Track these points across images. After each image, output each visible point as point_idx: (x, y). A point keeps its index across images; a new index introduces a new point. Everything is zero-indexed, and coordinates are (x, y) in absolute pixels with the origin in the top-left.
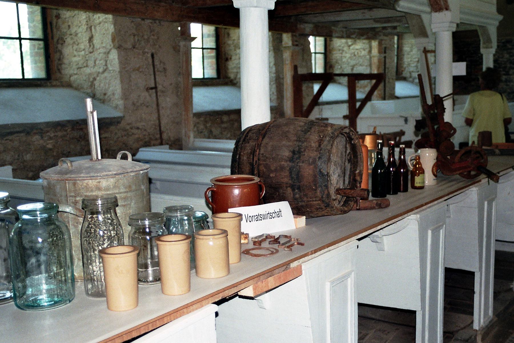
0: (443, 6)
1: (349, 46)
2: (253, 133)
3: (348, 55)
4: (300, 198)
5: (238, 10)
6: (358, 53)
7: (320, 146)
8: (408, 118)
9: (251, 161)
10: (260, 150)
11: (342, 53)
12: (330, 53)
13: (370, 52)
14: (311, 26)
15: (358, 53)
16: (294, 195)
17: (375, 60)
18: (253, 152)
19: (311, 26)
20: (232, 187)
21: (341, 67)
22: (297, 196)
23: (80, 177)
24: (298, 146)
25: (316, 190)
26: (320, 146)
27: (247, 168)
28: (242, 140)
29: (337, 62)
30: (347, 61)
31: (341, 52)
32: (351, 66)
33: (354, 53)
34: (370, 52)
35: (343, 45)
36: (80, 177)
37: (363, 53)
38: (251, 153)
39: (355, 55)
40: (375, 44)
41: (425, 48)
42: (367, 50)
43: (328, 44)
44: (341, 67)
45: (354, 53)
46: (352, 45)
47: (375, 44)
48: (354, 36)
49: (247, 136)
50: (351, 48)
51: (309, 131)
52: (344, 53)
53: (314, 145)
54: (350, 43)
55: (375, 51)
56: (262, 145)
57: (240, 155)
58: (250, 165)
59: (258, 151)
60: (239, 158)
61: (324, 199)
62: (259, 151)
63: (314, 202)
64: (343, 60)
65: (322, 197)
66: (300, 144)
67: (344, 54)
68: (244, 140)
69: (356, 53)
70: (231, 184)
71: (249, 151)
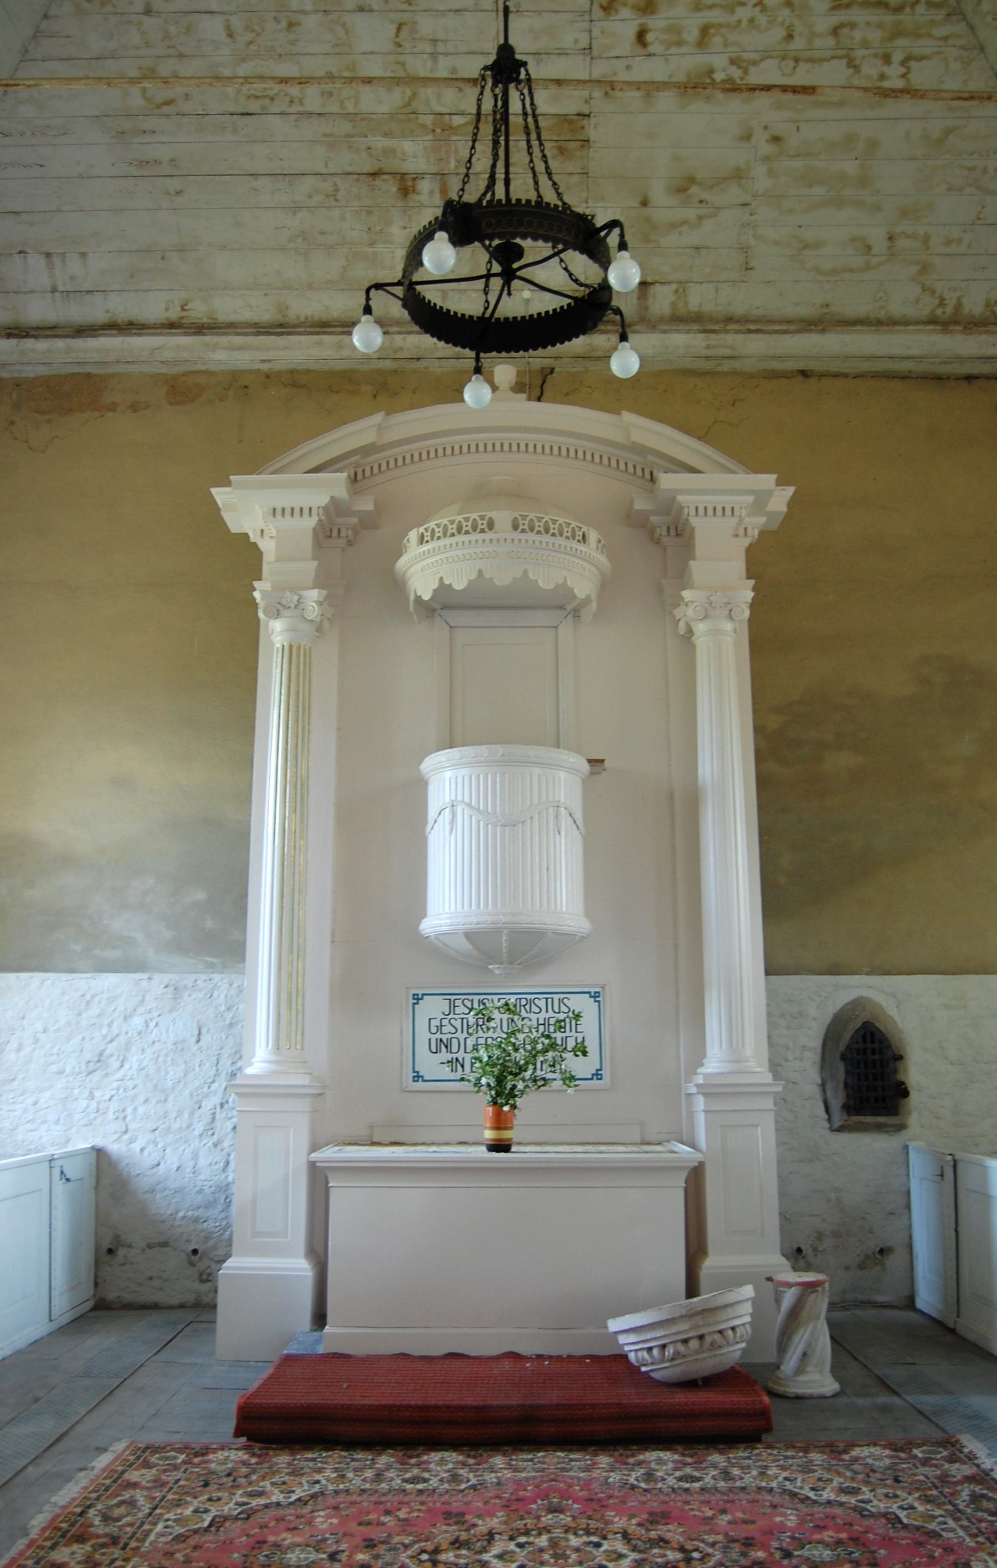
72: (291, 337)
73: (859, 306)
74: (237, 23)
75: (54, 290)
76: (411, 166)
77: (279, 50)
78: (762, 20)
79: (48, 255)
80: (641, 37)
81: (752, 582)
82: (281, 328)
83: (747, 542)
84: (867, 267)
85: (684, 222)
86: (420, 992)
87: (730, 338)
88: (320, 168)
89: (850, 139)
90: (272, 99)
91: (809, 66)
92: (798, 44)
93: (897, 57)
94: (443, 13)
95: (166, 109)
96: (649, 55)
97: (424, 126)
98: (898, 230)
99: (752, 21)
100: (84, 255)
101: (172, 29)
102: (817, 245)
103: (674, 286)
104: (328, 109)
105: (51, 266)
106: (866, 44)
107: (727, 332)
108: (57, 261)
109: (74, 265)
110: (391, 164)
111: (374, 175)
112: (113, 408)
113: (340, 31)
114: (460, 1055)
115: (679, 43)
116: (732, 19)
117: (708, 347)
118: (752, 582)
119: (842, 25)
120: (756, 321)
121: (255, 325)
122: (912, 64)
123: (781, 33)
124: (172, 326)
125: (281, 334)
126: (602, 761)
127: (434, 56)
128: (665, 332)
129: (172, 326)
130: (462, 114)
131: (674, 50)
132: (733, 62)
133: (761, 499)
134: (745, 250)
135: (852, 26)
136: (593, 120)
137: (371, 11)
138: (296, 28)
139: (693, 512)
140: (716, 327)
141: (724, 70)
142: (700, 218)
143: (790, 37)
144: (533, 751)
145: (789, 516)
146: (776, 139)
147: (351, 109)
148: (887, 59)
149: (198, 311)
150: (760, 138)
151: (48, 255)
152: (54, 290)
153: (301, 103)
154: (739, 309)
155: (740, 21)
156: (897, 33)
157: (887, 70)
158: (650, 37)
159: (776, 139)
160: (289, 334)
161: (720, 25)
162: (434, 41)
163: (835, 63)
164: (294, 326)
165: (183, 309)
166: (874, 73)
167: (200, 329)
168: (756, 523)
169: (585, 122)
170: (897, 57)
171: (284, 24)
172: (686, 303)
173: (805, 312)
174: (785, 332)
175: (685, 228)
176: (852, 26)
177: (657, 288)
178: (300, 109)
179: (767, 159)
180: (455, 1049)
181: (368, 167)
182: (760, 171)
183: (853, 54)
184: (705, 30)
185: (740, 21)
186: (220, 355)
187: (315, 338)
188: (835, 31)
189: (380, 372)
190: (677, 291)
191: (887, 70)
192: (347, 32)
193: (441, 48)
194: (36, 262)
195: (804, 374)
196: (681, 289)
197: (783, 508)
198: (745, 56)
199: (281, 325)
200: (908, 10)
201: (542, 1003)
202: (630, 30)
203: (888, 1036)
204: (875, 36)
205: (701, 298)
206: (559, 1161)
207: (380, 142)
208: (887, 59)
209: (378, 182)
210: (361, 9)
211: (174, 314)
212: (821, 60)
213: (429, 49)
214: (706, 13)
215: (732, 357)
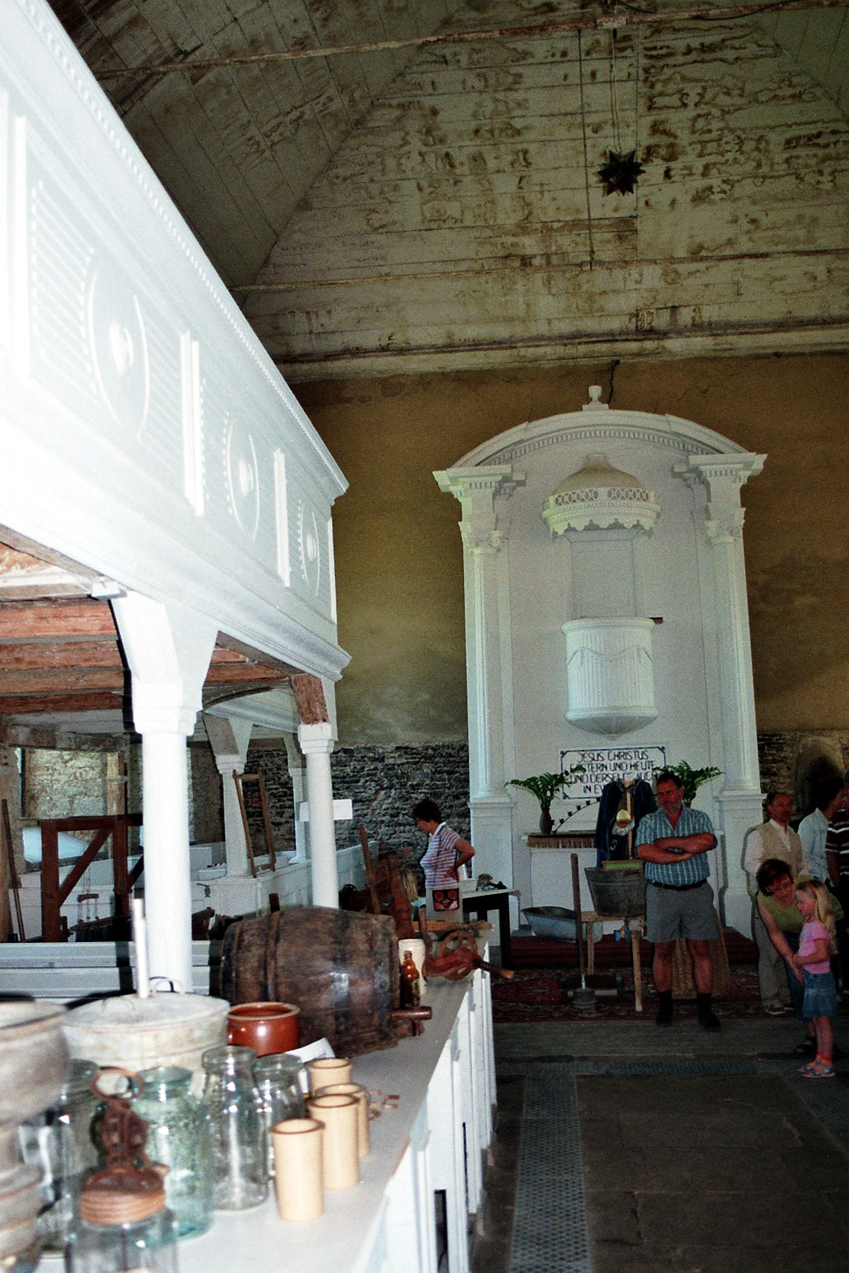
0: (320, 717)
1: (67, 762)
2: (252, 935)
3: (64, 778)
4: (346, 1029)
5: (140, 736)
6: (81, 773)
7: (371, 947)
8: (211, 888)
9: (262, 979)
10: (276, 960)
11: (52, 775)
12: (31, 773)
13: (103, 772)
14: (27, 730)
15: (81, 773)
16: (338, 1026)
17: (114, 787)
18: (264, 965)
19: (27, 730)
20: (256, 1023)
21: (51, 798)
22: (342, 1027)
23: (164, 1024)
24: (340, 951)
25: (372, 1015)
26: (371, 947)
27: (255, 992)
28: (235, 946)
29: (43, 790)
30: (62, 787)
31: (50, 771)
32: (69, 797)
33: (75, 773)
34: (103, 772)
35: (54, 761)
36: (164, 1024)
37: (91, 774)
38: (259, 967)
39: (76, 778)
40: (112, 759)
41: (234, 771)
42: (98, 770)
43: (27, 759)
44: (51, 798)
45: (75, 773)
46: (71, 759)
47: (112, 759)
48: (85, 747)
49: (243, 941)
50: (69, 764)
51: (347, 927)
52: (56, 773)
53: (363, 947)
54: (67, 758)
55: (113, 771)
56: (279, 952)
57: (237, 972)
58: (261, 986)
59: (272, 963)
60: (237, 976)
61: (383, 1028)
62: (276, 963)
63: (367, 1034)
64: (55, 787)
65: (381, 1025)
66: (342, 947)
67: (56, 776)
68: (239, 947)
69: (78, 774)
70: (253, 1019)
71: (256, 964)
72: (457, 354)
73: (812, 312)
74: (424, 183)
75: (311, 332)
76: (528, 252)
77: (449, 195)
78: (742, 159)
79: (308, 313)
80: (667, 174)
81: (744, 509)
82: (450, 347)
83: (741, 485)
84: (815, 288)
85: (698, 271)
86: (565, 750)
87: (730, 339)
88: (474, 256)
89: (800, 218)
90: (444, 221)
91: (772, 180)
92: (764, 170)
93: (827, 170)
94: (545, 170)
95: (380, 231)
96: (673, 182)
97: (537, 229)
98: (833, 266)
99: (735, 159)
100: (329, 312)
101: (386, 189)
102: (781, 279)
103: (693, 307)
104: (478, 224)
105: (309, 320)
106: (807, 166)
107: (727, 335)
108: (313, 316)
109: (324, 319)
110: (514, 251)
111: (506, 257)
112: (349, 401)
113: (486, 184)
114: (588, 784)
115: (691, 175)
116: (723, 160)
117: (715, 345)
118: (744, 509)
119: (791, 157)
120: (744, 325)
121: (433, 347)
122: (836, 174)
123: (754, 164)
124: (383, 350)
125: (451, 352)
126: (661, 619)
127: (542, 193)
128: (689, 337)
129: (383, 350)
130: (559, 221)
131: (687, 178)
132: (724, 182)
133: (747, 465)
134: (737, 283)
135: (798, 157)
136: (639, 219)
137: (504, 171)
138: (460, 184)
139: (708, 475)
140: (719, 332)
141: (719, 186)
142: (707, 268)
143: (759, 166)
144: (623, 621)
145: (764, 472)
146: (753, 221)
147: (491, 223)
148: (821, 173)
149: (399, 340)
150: (743, 221)
151: (308, 313)
152: (311, 332)
153: (461, 222)
154: (734, 318)
155: (728, 160)
156: (827, 158)
157: (821, 179)
158: (672, 173)
159: (753, 221)
160: (455, 351)
161: (715, 163)
162: (542, 185)
163: (787, 178)
164: (458, 346)
165: (389, 339)
166: (813, 182)
167: (401, 351)
168: (745, 475)
169: (634, 220)
170: (827, 170)
171: (452, 182)
172: (701, 317)
173: (776, 317)
174: (763, 333)
175: (698, 274)
176: (798, 157)
177: (682, 309)
178: (462, 225)
179: (748, 232)
180: (585, 780)
181: (501, 254)
182: (744, 239)
183: (799, 172)
184: (706, 167)
185: (728, 160)
186: (414, 366)
187: (473, 353)
188: (787, 161)
189: (513, 370)
190: (694, 310)
191: (821, 179)
192: (490, 184)
193: (546, 188)
194: (301, 317)
195: (778, 355)
196: (697, 309)
197: (761, 466)
198: (731, 178)
199: (450, 346)
200: (832, 146)
201: (633, 755)
202: (662, 170)
203: (133, 970)
204: (813, 162)
205: (710, 313)
206: (477, 1054)
207: (510, 240)
208: (821, 173)
209: (508, 262)
210: (498, 172)
211: (384, 342)
212: (779, 177)
213: (538, 188)
214: (707, 157)
215: (730, 349)
